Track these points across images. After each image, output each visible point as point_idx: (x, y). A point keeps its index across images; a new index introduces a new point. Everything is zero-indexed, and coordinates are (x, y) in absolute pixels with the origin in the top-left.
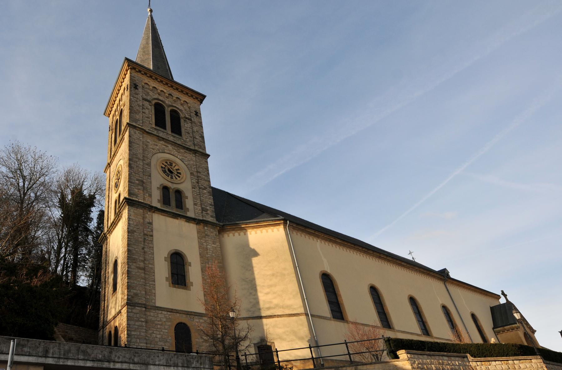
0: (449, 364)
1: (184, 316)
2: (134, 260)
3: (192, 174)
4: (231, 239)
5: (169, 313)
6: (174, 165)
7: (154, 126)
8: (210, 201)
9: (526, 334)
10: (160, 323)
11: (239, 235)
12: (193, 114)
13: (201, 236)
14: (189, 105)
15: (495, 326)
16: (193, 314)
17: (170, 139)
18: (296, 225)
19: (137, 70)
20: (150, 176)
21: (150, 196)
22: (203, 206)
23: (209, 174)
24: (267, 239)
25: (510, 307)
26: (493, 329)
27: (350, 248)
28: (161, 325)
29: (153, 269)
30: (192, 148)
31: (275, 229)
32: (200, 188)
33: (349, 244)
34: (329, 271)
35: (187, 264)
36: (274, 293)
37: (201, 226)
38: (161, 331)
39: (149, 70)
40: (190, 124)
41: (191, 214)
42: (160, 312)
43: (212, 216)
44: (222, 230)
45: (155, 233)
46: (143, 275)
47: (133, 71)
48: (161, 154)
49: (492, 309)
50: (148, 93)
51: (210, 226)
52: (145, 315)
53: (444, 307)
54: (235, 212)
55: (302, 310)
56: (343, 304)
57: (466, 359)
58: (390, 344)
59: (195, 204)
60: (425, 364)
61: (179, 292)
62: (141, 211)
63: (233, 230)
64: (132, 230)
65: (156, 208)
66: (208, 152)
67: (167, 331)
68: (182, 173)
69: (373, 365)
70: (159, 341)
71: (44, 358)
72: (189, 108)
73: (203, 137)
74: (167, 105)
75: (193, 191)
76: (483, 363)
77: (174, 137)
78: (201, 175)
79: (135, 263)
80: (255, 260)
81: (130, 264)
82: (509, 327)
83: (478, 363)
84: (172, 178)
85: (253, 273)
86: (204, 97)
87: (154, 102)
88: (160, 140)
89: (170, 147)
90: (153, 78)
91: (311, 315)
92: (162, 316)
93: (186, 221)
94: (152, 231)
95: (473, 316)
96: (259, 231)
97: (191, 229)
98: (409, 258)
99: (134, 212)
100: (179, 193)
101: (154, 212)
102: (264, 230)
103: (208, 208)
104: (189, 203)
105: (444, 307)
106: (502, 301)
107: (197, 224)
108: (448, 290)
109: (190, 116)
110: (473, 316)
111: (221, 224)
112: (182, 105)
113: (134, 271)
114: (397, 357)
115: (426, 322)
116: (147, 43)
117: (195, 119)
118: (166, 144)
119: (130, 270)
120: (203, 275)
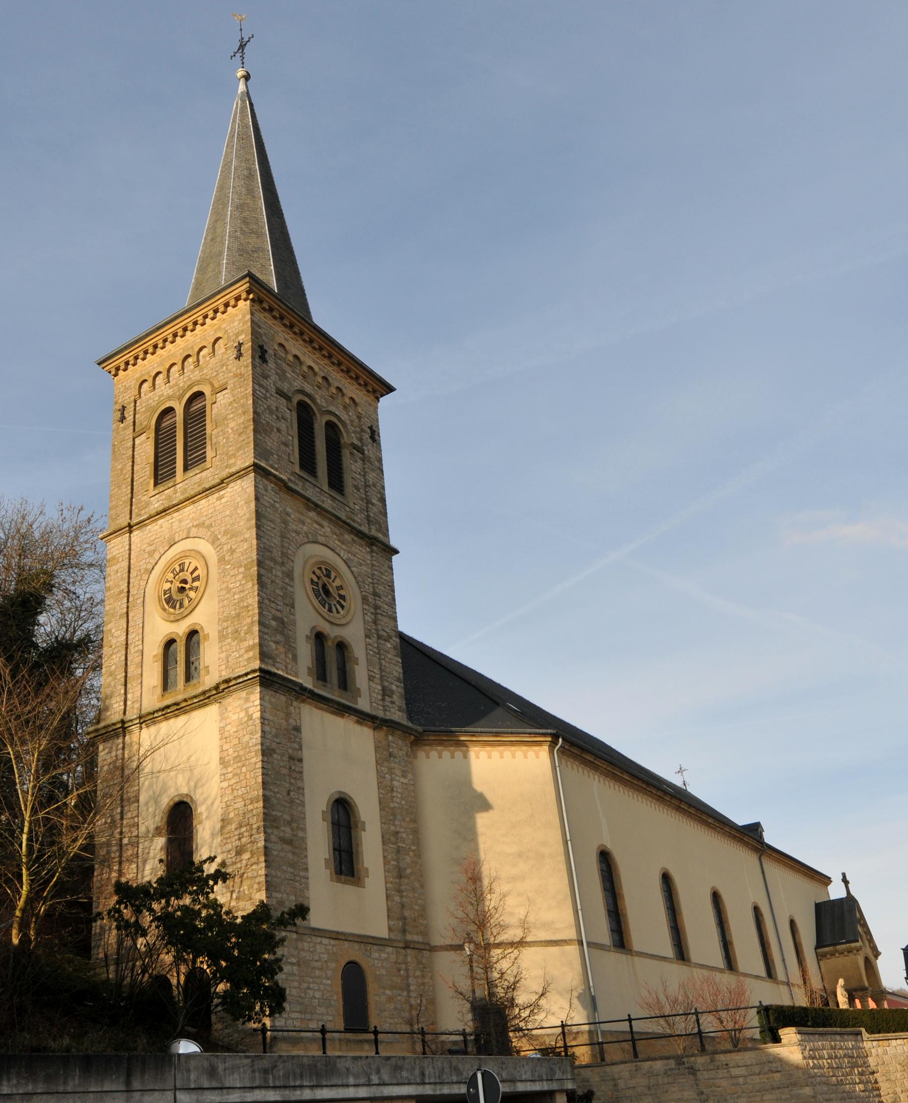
0: (841, 1048)
1: (356, 946)
2: (275, 821)
3: (365, 599)
4: (434, 763)
5: (333, 942)
6: (333, 575)
7: (297, 469)
8: (396, 669)
9: (867, 961)
10: (318, 964)
11: (453, 757)
12: (366, 436)
13: (384, 757)
14: (360, 410)
15: (819, 944)
16: (371, 941)
17: (325, 506)
18: (579, 749)
19: (266, 306)
20: (293, 606)
21: (295, 658)
22: (386, 684)
23: (394, 600)
24: (507, 772)
25: (849, 905)
26: (817, 948)
27: (639, 791)
28: (321, 969)
29: (303, 839)
30: (364, 529)
31: (531, 752)
32: (379, 637)
33: (640, 783)
34: (609, 846)
35: (359, 825)
36: (520, 894)
37: (381, 734)
38: (322, 983)
39: (269, 291)
40: (360, 463)
41: (363, 704)
42: (319, 940)
43: (400, 710)
44: (418, 740)
45: (306, 754)
46: (290, 856)
47: (257, 307)
48: (318, 549)
49: (819, 907)
50: (284, 372)
51: (400, 733)
52: (296, 948)
53: (756, 909)
54: (450, 701)
55: (572, 934)
56: (625, 916)
57: (859, 1037)
58: (768, 1016)
59: (371, 678)
60: (817, 1050)
61: (347, 891)
62: (283, 698)
63: (441, 743)
64: (268, 749)
65: (303, 689)
66: (394, 542)
67: (329, 982)
68: (347, 598)
69: (741, 1053)
70: (319, 1005)
71: (422, 1086)
72: (359, 417)
73: (383, 500)
74: (319, 410)
75: (367, 644)
76: (881, 1043)
77: (333, 499)
78: (381, 600)
79: (277, 828)
80: (482, 820)
81: (269, 831)
82: (844, 946)
83: (875, 1043)
84: (330, 610)
85: (476, 850)
86: (390, 389)
87: (297, 398)
88: (309, 509)
89: (327, 528)
90: (296, 330)
91: (588, 943)
92: (323, 946)
93: (358, 722)
94: (301, 749)
95: (792, 923)
96: (495, 752)
97: (362, 739)
98: (677, 781)
99: (271, 703)
100: (342, 646)
101: (303, 701)
102: (508, 751)
103: (394, 688)
104: (361, 674)
105: (756, 909)
106: (836, 892)
107: (375, 729)
108: (763, 873)
109: (361, 440)
110: (792, 923)
111: (420, 729)
112: (333, 399)
113: (276, 848)
114: (777, 1040)
115: (731, 944)
116: (250, 192)
117: (369, 450)
118: (319, 519)
119: (269, 845)
120: (384, 850)
